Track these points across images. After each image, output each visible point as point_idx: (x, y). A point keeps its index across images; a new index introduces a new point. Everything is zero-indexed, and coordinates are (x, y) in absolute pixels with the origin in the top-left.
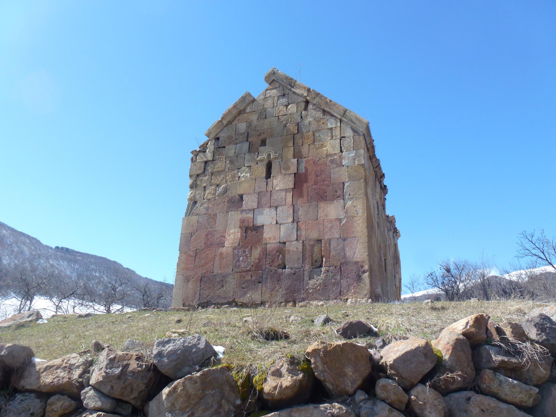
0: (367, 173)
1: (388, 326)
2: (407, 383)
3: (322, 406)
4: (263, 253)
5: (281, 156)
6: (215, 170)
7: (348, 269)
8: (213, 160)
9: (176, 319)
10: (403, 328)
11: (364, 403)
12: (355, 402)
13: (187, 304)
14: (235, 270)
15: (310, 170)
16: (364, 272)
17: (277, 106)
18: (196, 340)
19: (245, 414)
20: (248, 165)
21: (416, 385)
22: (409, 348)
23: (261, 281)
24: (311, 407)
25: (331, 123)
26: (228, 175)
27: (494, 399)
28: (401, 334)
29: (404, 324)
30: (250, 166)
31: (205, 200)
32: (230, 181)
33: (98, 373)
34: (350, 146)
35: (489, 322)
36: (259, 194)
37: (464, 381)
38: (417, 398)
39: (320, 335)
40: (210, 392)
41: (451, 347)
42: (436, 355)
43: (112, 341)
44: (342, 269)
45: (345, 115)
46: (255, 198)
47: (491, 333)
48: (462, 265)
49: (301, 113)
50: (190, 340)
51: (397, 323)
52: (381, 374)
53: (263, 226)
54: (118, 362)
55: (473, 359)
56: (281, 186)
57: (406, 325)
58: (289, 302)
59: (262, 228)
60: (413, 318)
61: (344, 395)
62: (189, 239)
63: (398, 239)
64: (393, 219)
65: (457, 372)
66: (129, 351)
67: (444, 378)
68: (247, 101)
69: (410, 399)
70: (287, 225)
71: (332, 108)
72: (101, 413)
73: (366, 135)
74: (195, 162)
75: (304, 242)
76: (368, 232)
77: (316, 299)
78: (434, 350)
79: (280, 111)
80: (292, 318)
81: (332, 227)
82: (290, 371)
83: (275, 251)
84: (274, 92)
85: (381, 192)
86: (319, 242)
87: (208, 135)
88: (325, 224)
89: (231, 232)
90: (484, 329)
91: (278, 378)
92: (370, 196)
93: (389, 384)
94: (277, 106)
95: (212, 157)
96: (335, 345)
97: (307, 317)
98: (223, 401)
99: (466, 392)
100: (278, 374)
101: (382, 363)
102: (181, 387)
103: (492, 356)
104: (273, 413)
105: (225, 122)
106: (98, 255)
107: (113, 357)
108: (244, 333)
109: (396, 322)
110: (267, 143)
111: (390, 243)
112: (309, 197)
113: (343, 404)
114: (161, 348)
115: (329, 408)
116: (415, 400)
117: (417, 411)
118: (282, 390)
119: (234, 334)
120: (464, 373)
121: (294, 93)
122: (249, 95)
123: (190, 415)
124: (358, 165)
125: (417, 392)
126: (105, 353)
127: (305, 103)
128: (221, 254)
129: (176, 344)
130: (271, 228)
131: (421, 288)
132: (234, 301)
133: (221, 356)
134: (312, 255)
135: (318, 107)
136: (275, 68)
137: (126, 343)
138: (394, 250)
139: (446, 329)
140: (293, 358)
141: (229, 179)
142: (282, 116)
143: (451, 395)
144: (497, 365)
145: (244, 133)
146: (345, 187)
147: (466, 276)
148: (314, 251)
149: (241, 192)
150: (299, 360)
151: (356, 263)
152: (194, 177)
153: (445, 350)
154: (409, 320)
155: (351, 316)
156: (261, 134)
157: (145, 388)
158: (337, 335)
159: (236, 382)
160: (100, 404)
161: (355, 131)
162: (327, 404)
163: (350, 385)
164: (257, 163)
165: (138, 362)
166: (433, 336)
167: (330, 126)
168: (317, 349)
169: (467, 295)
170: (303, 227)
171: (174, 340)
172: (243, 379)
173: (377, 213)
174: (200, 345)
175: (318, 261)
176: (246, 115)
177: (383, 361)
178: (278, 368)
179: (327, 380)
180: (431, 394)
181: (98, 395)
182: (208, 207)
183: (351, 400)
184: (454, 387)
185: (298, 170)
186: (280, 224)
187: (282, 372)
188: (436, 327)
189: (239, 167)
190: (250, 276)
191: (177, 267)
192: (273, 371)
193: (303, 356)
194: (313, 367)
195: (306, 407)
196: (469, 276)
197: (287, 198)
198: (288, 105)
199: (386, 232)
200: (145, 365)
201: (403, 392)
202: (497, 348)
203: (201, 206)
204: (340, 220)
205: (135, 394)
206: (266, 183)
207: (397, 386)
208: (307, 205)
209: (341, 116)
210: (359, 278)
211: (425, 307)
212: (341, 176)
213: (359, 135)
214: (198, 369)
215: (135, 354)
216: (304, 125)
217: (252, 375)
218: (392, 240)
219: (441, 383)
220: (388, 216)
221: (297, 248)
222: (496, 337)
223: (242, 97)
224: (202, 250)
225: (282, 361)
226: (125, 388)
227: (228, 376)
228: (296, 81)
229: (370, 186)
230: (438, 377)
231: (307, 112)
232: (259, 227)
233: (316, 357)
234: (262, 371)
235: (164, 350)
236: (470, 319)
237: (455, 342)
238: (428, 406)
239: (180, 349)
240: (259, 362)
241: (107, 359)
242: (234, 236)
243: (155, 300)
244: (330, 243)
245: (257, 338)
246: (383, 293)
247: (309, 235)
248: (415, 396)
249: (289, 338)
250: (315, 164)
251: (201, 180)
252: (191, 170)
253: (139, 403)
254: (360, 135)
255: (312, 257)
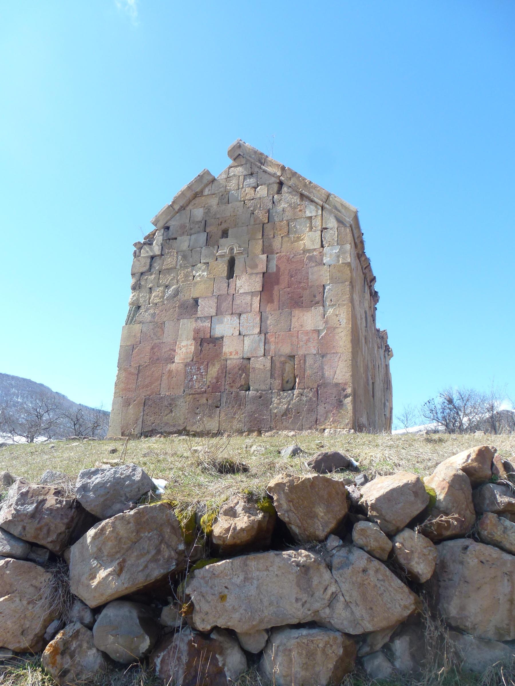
0: (354, 275)
1: (372, 460)
2: (391, 528)
3: (285, 554)
4: (222, 371)
5: (247, 252)
6: (164, 267)
7: (326, 392)
8: (162, 255)
9: (110, 448)
10: (390, 462)
11: (338, 551)
12: (326, 549)
13: (127, 432)
14: (188, 391)
15: (282, 269)
16: (346, 396)
17: (243, 188)
18: (130, 470)
19: (190, 562)
20: (205, 261)
21: (403, 530)
22: (395, 485)
23: (219, 405)
24: (272, 554)
25: (310, 211)
26: (180, 273)
27: (496, 548)
28: (387, 469)
29: (391, 458)
30: (208, 263)
31: (151, 305)
32: (183, 282)
33: (7, 510)
34: (333, 239)
35: (496, 455)
36: (218, 297)
37: (461, 527)
38: (403, 545)
39: (286, 468)
40: (146, 534)
41: (448, 485)
42: (428, 494)
43: (28, 474)
44: (319, 392)
45: (328, 200)
46: (213, 302)
47: (497, 468)
48: (467, 395)
49: (273, 197)
50: (123, 471)
51: (384, 457)
52: (360, 516)
53: (222, 338)
54: (32, 497)
55: (473, 501)
56: (246, 288)
57: (394, 459)
58: (253, 431)
59: (221, 340)
60: (403, 451)
61: (312, 541)
62: (131, 353)
63: (390, 360)
64: (385, 335)
65: (453, 515)
66: (46, 484)
67: (436, 522)
68: (205, 181)
69: (394, 547)
70: (252, 337)
71: (312, 192)
72: (10, 559)
73: (353, 226)
74: (138, 256)
75: (273, 358)
76: (353, 348)
77: (286, 428)
78: (426, 488)
79: (246, 195)
80: (254, 448)
81: (308, 340)
82: (246, 510)
83: (237, 369)
84: (239, 170)
85: (371, 299)
86: (292, 359)
87: (155, 223)
88: (299, 337)
89: (182, 344)
90: (489, 464)
91: (232, 518)
92: (357, 303)
93: (369, 528)
94: (243, 188)
95: (160, 250)
96: (303, 479)
97: (273, 446)
98: (163, 546)
99: (463, 540)
100: (231, 513)
101: (362, 502)
102: (110, 528)
103: (496, 497)
104: (224, 561)
105: (177, 207)
106: (21, 376)
107: (25, 491)
108: (192, 464)
109: (381, 455)
110: (229, 234)
111: (380, 363)
112: (280, 303)
113: (312, 551)
114: (86, 480)
115: (293, 556)
116: (400, 548)
117: (402, 561)
118: (236, 533)
119: (180, 465)
120: (462, 517)
121: (265, 172)
122: (208, 173)
123: (120, 562)
124: (342, 263)
125: (403, 539)
126: (15, 486)
127: (278, 185)
128: (170, 372)
129: (105, 475)
130: (232, 340)
131: (417, 421)
132: (185, 429)
133: (161, 491)
134: (283, 374)
135: (294, 190)
136: (241, 140)
137: (44, 475)
138: (384, 373)
139: (442, 463)
140: (251, 494)
141: (181, 279)
142: (249, 200)
143: (445, 543)
144: (502, 508)
145: (201, 222)
146: (326, 291)
147: (472, 408)
148: (285, 370)
149: (195, 296)
150: (258, 497)
151: (337, 385)
152: (138, 275)
153: (440, 489)
154: (398, 453)
155: (327, 447)
156: (221, 222)
157: (66, 529)
158: (308, 468)
159: (179, 522)
160: (9, 549)
161: (339, 221)
162: (291, 551)
163: (321, 528)
164: (217, 259)
165: (56, 498)
166: (427, 472)
167: (308, 214)
168: (282, 483)
169: (473, 428)
170: (272, 339)
171: (103, 470)
172: (188, 518)
173: (364, 324)
174: (135, 476)
175: (289, 382)
176: (203, 198)
177: (363, 500)
178: (232, 505)
179: (292, 523)
180: (420, 541)
181: (7, 537)
182: (155, 313)
183: (321, 547)
184: (448, 533)
185: (268, 268)
186: (244, 336)
187: (237, 511)
188: (431, 461)
189: (194, 264)
190: (205, 399)
191: (115, 388)
192: (226, 510)
193: (263, 492)
194: (276, 505)
195: (266, 554)
196: (475, 408)
197: (253, 303)
198: (256, 186)
199: (376, 349)
200: (66, 501)
201: (386, 538)
202: (504, 488)
203: (145, 311)
204: (319, 332)
205: (53, 537)
206: (227, 285)
207: (379, 531)
208: (278, 312)
209: (324, 202)
210: (340, 404)
211: (419, 438)
212: (321, 277)
213: (345, 226)
214: (131, 506)
215: (53, 487)
216: (276, 212)
217: (200, 514)
218: (383, 360)
219: (432, 528)
220: (378, 331)
221: (264, 366)
222: (503, 474)
223: (199, 176)
224: (147, 366)
225: (237, 497)
226: (40, 529)
227: (169, 515)
228: (267, 157)
229: (357, 291)
230: (429, 521)
231: (280, 195)
232: (217, 339)
233: (280, 493)
234: (212, 509)
235: (90, 483)
236: (472, 451)
237: (453, 478)
238: (416, 555)
239: (111, 481)
240: (208, 498)
241: (18, 493)
242: (186, 349)
243: (90, 429)
244: (305, 361)
245: (208, 471)
246: (369, 423)
247: (279, 350)
248: (400, 543)
249: (249, 472)
250: (290, 262)
251: (146, 279)
252: (133, 266)
253: (58, 548)
254: (346, 226)
255: (282, 376)
